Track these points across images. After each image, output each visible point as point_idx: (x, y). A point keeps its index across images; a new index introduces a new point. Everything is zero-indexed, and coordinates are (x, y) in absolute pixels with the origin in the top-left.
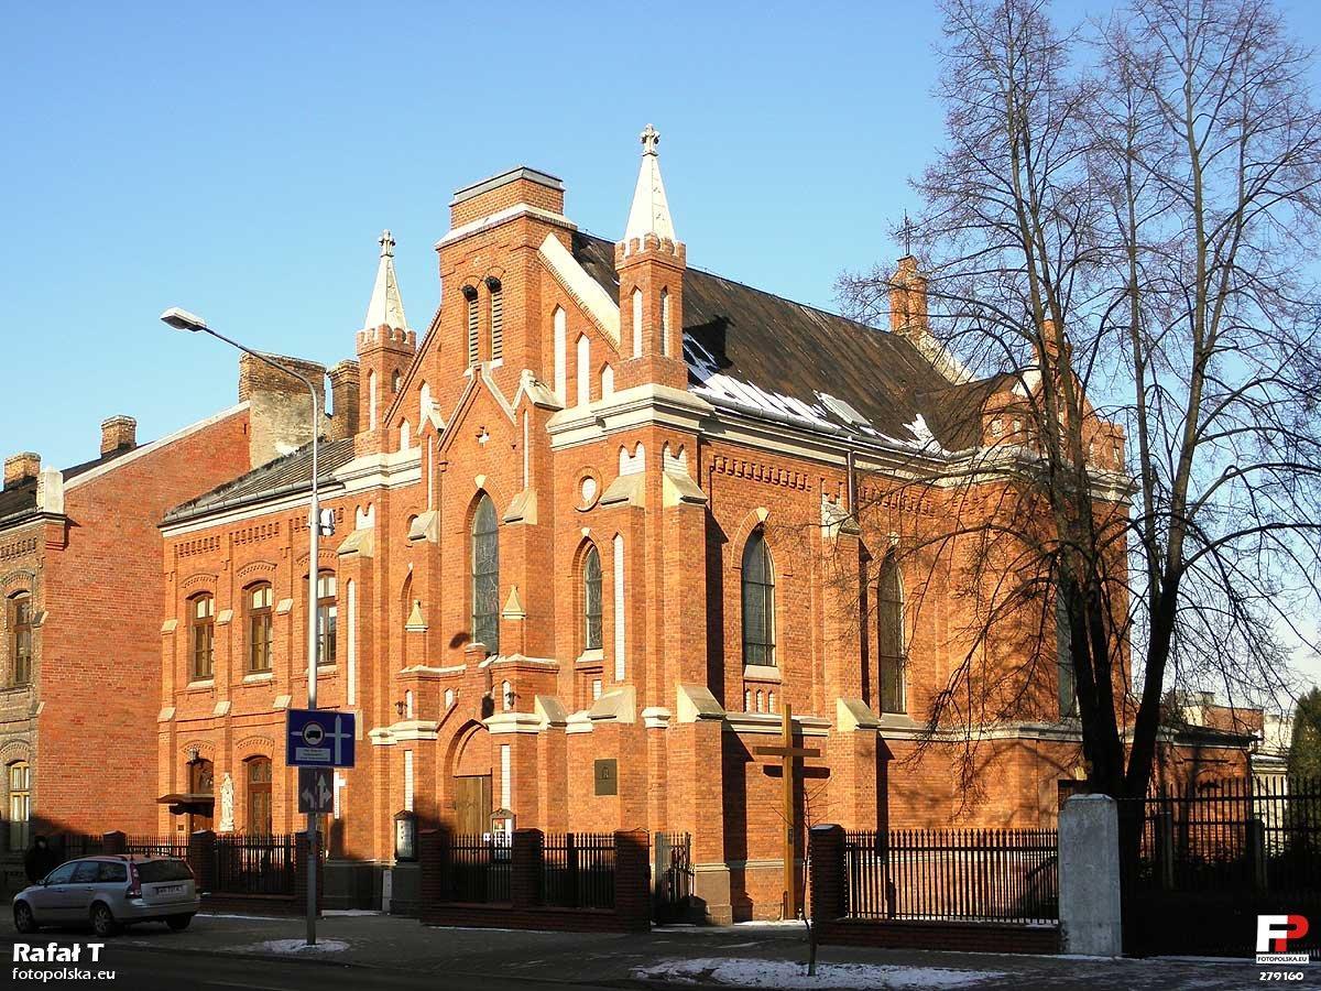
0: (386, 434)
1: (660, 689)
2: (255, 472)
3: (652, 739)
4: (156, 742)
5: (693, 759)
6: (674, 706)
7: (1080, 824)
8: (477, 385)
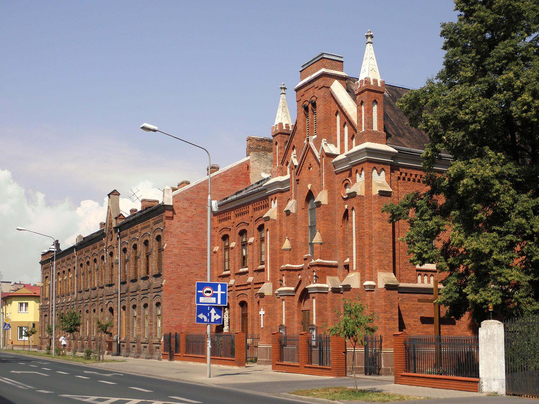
2: (252, 185)
7: (487, 334)
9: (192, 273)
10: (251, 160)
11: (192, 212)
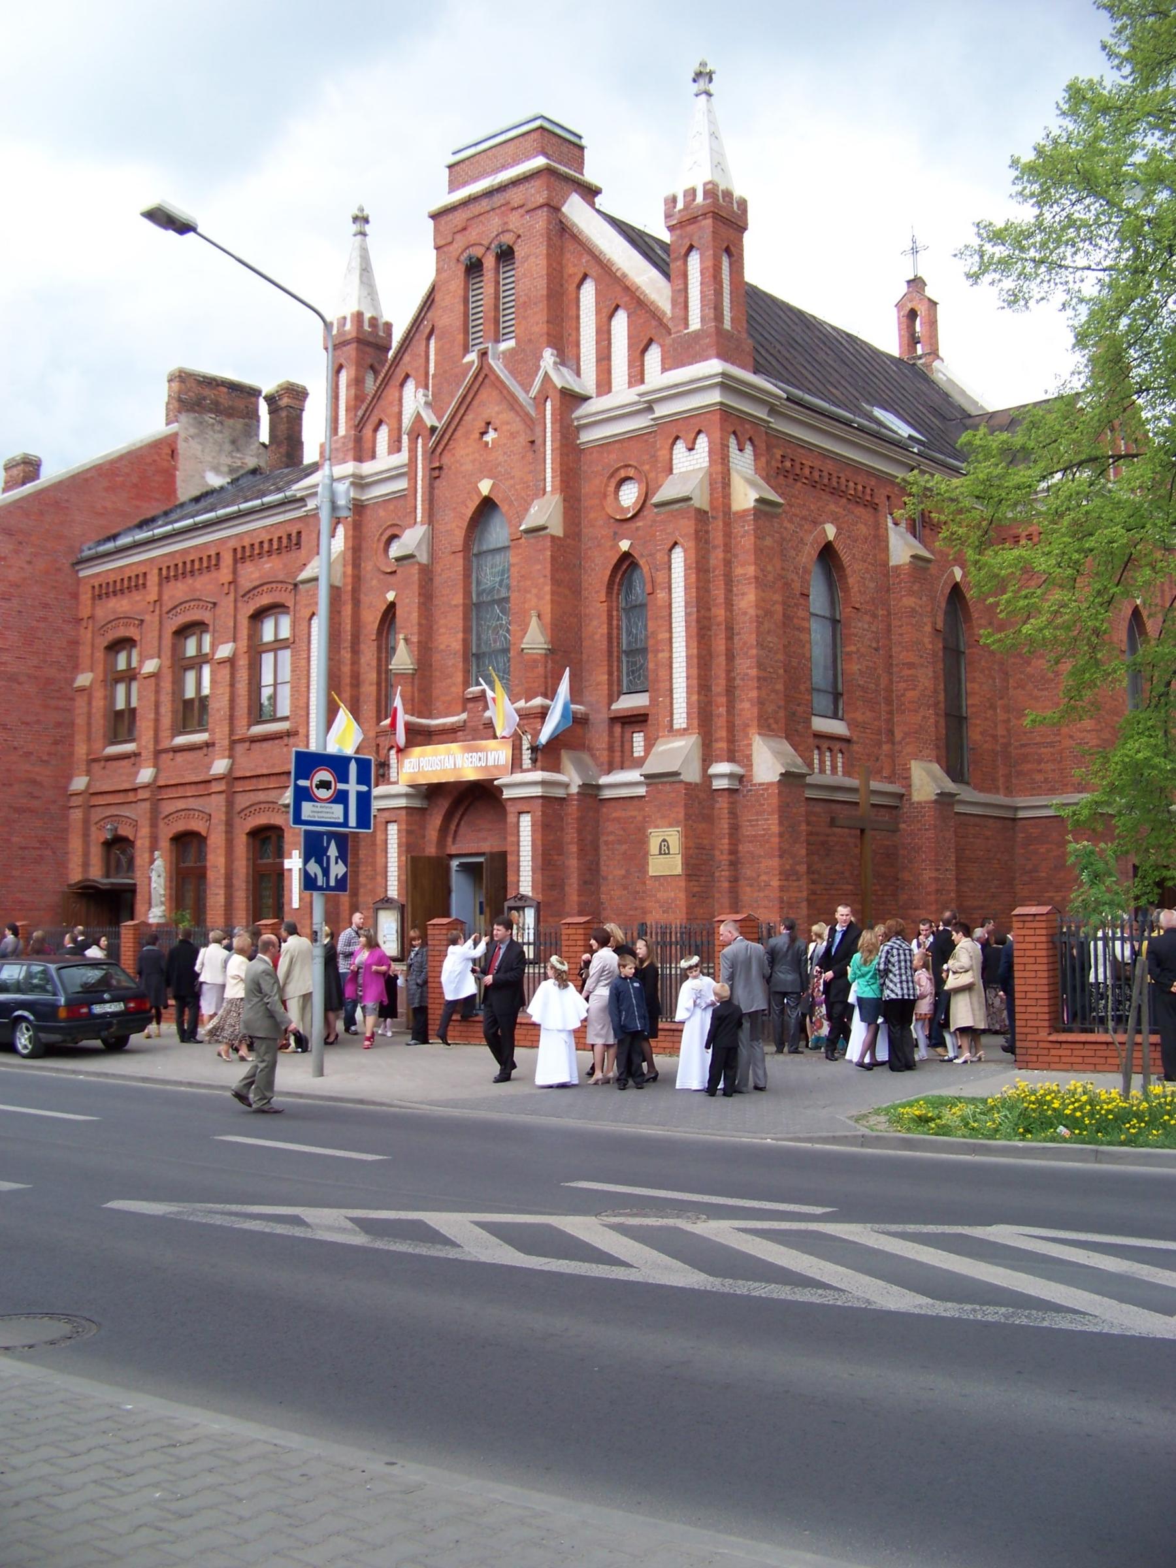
0: (358, 440)
1: (731, 740)
2: (182, 505)
3: (722, 803)
4: (65, 818)
5: (775, 829)
6: (747, 762)
8: (483, 375)
9: (15, 748)
10: (182, 435)
11: (22, 568)
